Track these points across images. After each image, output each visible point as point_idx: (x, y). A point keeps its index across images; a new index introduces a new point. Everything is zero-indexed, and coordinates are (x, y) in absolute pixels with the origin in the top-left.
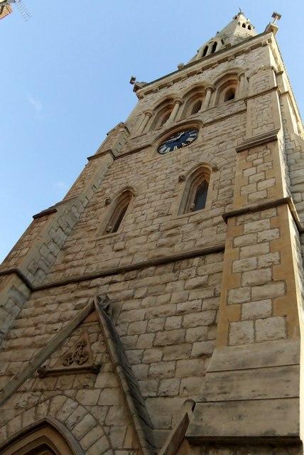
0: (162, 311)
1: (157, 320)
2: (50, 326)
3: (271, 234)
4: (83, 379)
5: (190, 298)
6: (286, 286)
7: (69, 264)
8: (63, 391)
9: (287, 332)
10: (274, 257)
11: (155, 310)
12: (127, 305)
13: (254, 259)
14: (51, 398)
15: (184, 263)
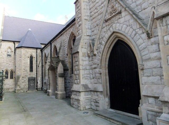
2: (100, 7)
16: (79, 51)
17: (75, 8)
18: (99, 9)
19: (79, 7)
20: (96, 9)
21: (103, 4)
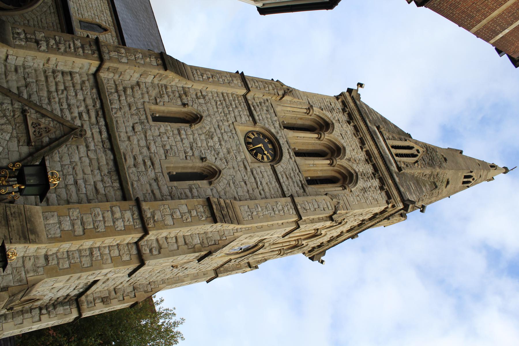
0: (78, 172)
1: (70, 169)
2: (65, 100)
3: (120, 224)
4: (23, 139)
5: (87, 186)
6: (81, 236)
7: (122, 93)
8: (15, 129)
9: (52, 238)
10: (101, 229)
11: (78, 168)
12: (83, 149)
13: (102, 219)
14: (10, 123)
15: (115, 177)
18: (61, 96)
20: (65, 88)
21: (66, 107)
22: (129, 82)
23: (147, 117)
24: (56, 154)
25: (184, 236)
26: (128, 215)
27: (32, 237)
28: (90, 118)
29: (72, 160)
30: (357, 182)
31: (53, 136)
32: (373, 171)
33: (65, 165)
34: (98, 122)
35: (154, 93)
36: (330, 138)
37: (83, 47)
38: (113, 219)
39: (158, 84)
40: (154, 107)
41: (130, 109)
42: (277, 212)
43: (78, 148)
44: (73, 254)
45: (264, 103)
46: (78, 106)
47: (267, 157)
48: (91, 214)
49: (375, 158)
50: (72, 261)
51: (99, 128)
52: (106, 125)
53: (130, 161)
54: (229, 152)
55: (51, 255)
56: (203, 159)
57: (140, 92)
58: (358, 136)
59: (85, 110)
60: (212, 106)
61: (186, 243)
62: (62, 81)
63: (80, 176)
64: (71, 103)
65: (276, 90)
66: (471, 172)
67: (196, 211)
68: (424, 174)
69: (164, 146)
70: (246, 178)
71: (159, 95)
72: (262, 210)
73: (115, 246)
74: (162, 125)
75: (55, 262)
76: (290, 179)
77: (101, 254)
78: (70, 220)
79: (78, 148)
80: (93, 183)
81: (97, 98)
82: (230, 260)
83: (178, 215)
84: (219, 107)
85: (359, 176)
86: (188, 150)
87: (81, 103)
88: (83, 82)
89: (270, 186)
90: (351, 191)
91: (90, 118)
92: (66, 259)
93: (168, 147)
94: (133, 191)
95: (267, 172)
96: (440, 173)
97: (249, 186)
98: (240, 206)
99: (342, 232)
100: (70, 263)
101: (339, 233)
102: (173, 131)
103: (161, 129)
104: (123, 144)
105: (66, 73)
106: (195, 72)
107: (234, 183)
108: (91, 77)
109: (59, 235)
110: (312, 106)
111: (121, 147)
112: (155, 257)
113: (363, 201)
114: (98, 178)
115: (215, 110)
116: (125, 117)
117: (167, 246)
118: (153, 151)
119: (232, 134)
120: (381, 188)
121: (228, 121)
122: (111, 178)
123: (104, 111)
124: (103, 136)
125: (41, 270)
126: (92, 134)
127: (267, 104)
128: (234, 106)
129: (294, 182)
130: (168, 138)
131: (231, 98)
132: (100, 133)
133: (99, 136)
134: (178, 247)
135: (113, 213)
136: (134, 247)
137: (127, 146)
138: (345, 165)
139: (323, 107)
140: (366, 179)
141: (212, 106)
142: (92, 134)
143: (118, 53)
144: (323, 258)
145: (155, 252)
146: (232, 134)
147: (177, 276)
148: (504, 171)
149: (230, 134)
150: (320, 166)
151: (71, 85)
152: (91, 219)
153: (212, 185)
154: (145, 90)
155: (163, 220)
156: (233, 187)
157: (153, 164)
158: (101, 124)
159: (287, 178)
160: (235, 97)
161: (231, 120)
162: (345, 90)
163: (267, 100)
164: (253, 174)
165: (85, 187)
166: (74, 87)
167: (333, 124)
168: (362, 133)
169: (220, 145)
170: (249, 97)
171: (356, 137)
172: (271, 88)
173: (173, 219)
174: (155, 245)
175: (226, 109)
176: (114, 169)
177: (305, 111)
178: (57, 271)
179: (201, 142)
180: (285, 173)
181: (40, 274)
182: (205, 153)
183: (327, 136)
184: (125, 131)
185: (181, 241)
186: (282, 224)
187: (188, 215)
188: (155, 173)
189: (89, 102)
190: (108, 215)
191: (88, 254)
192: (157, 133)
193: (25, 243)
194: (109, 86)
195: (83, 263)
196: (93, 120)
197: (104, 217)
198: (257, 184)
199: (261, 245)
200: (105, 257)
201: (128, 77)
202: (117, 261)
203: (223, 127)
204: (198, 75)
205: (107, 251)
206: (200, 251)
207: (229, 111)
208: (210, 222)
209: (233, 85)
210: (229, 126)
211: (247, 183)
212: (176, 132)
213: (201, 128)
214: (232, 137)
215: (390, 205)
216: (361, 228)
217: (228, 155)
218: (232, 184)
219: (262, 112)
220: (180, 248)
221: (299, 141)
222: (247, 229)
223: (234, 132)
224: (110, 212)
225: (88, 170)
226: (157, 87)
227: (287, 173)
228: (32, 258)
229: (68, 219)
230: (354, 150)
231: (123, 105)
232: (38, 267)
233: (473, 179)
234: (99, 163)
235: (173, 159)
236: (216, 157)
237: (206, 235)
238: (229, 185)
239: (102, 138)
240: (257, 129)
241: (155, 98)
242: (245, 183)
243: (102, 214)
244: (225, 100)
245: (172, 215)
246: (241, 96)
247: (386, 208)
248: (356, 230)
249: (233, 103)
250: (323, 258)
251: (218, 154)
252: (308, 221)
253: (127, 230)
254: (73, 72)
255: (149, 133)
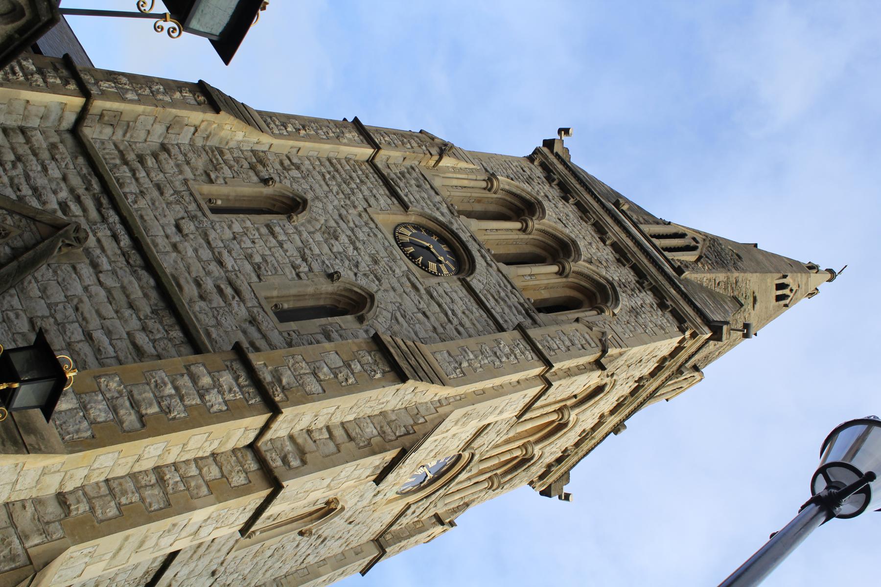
0: (87, 315)
1: (70, 311)
2: (23, 180)
5: (114, 342)
11: (87, 307)
12: (86, 270)
13: (173, 392)
15: (169, 320)
16: (222, 113)
17: (491, 157)
18: (14, 173)
19: (40, 82)
20: (19, 158)
21: (30, 192)
22: (145, 145)
23: (199, 206)
24: (30, 282)
25: (342, 424)
26: (226, 379)
27: (29, 439)
28: (85, 210)
29: (69, 293)
30: (617, 300)
31: (18, 243)
32: (637, 279)
33: (57, 304)
34: (104, 219)
35: (200, 163)
36: (543, 228)
37: (40, 71)
38: (198, 392)
39: (203, 147)
40: (207, 189)
41: (162, 194)
42: (504, 359)
43: (74, 268)
44: (121, 484)
45: (409, 172)
46: (57, 187)
47: (446, 266)
48: (148, 384)
49: (633, 254)
50: (124, 500)
51: (110, 229)
52: (124, 221)
53: (190, 290)
54: (376, 262)
55: (71, 492)
56: (332, 277)
57: (172, 163)
58: (589, 219)
59: (70, 197)
60: (318, 182)
61: (351, 438)
62: (7, 145)
63: (94, 323)
64: (38, 185)
65: (424, 147)
66: (785, 277)
67: (359, 362)
68: (717, 282)
69: (249, 257)
70: (423, 305)
71: (211, 167)
72: (476, 357)
73: (207, 457)
74: (234, 220)
75: (83, 507)
76: (502, 303)
77: (182, 478)
78: (105, 398)
79: (74, 268)
80: (125, 336)
81: (89, 174)
82: (408, 507)
83: (325, 373)
84: (330, 183)
85: (618, 289)
86: (299, 261)
87: (58, 184)
88: (53, 147)
89: (471, 316)
90: (614, 314)
91: (85, 210)
92: (109, 498)
93: (258, 259)
94: (212, 345)
95: (456, 292)
96: (740, 280)
97: (432, 319)
98: (433, 353)
99: (602, 416)
100: (119, 506)
101: (596, 421)
102: (258, 229)
103: (234, 226)
104: (167, 258)
105: (13, 129)
106: (269, 120)
107: (404, 317)
108: (68, 138)
109: (89, 433)
110: (493, 175)
111: (165, 265)
112: (297, 473)
113: (640, 330)
114: (134, 324)
115: (326, 188)
116: (157, 209)
117: (315, 448)
118: (230, 268)
119: (371, 229)
120: (662, 306)
121: (355, 207)
122: (161, 323)
123: (109, 195)
124: (122, 244)
125: (57, 531)
126: (99, 241)
127: (414, 175)
128: (358, 181)
129: (510, 307)
130: (253, 242)
131: (348, 167)
132: (115, 237)
133: (114, 244)
134: (338, 446)
135: (194, 379)
136: (249, 456)
137: (175, 262)
138: (586, 271)
139: (512, 176)
140: (630, 292)
141: (318, 182)
142: (99, 241)
143: (115, 83)
144: (566, 489)
145: (295, 463)
146: (371, 229)
147: (304, 565)
148: (829, 276)
149: (366, 229)
150: (542, 279)
151: (29, 152)
152: (151, 395)
153: (366, 323)
154: (181, 157)
155: (302, 385)
156: (405, 325)
157: (237, 292)
158: (111, 220)
159: (496, 300)
160: (356, 164)
161: (361, 205)
162: (541, 145)
163: (413, 168)
164: (432, 297)
165: (111, 344)
166: (35, 154)
167: (540, 203)
168: (594, 213)
169: (356, 248)
170: (378, 162)
171: (586, 222)
172: (415, 145)
173: (319, 381)
174: (289, 447)
175: (344, 185)
176: (161, 305)
177: (484, 184)
178: (93, 527)
179: (318, 246)
180: (488, 291)
181: (54, 537)
182: (332, 265)
183: (535, 224)
184: (162, 233)
185: (339, 433)
186: (518, 382)
187: (345, 371)
188: (247, 308)
189: (76, 181)
190: (185, 382)
191: (153, 481)
192: (228, 234)
193: (17, 452)
194: (107, 154)
195: (148, 500)
196: (93, 214)
197: (176, 388)
198: (446, 315)
199: (466, 455)
200: (193, 484)
201: (142, 135)
202: (222, 490)
203: (350, 218)
204: (277, 126)
205: (193, 471)
206: (383, 450)
207: (352, 190)
208: (394, 382)
209: (345, 141)
210: (360, 215)
211: (428, 313)
212: (264, 230)
213: (309, 222)
214: (372, 234)
215: (688, 334)
216: (637, 398)
217: (377, 267)
218: (401, 319)
219: (410, 189)
220: (342, 447)
221: (490, 237)
222: (458, 398)
223: (372, 225)
224: (186, 377)
225: (108, 311)
226: (204, 153)
227: (492, 291)
228: (28, 504)
229: (100, 397)
230: (590, 244)
231: (146, 186)
232: (48, 523)
233: (791, 290)
234: (128, 296)
235: (275, 280)
236: (355, 270)
237: (385, 417)
238: (397, 320)
239: (120, 248)
240: (412, 219)
241: (205, 172)
242: (424, 314)
243: (172, 383)
244: (337, 171)
245: (315, 374)
246: (363, 162)
247: (681, 342)
248: (628, 406)
249: (354, 175)
250: (566, 489)
251: (357, 266)
252: (560, 373)
253: (232, 412)
254: (27, 128)
255: (212, 235)
